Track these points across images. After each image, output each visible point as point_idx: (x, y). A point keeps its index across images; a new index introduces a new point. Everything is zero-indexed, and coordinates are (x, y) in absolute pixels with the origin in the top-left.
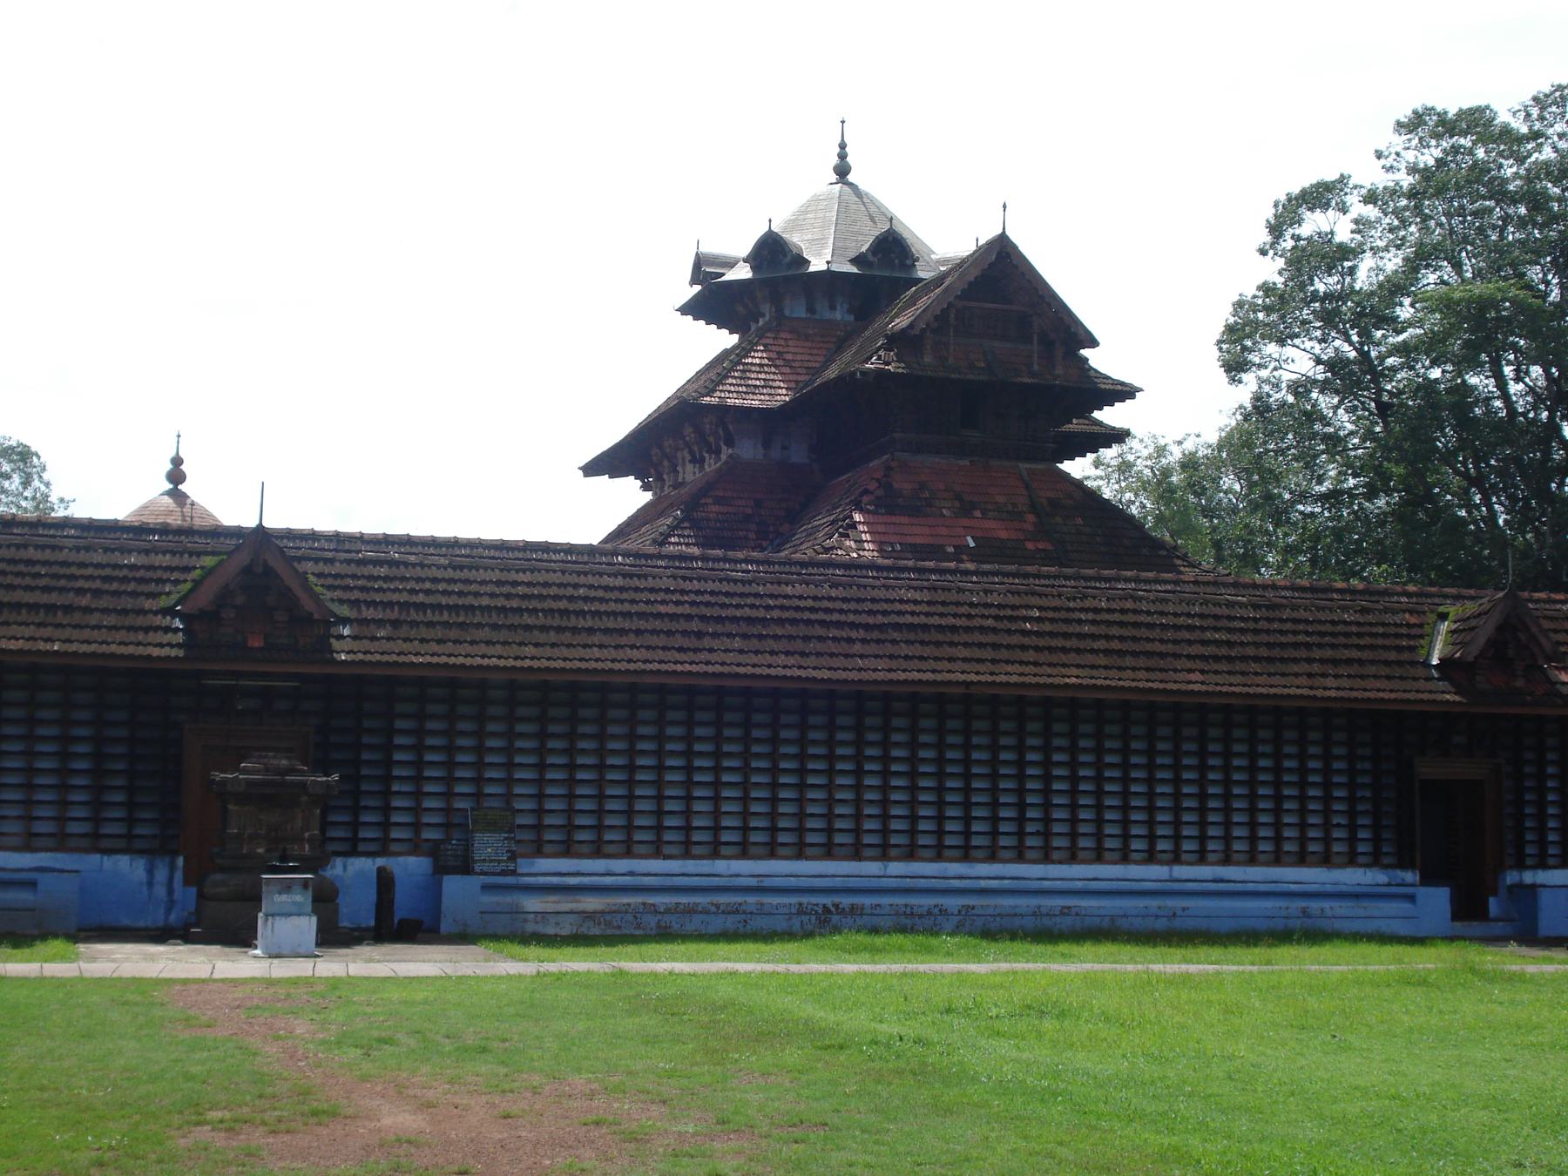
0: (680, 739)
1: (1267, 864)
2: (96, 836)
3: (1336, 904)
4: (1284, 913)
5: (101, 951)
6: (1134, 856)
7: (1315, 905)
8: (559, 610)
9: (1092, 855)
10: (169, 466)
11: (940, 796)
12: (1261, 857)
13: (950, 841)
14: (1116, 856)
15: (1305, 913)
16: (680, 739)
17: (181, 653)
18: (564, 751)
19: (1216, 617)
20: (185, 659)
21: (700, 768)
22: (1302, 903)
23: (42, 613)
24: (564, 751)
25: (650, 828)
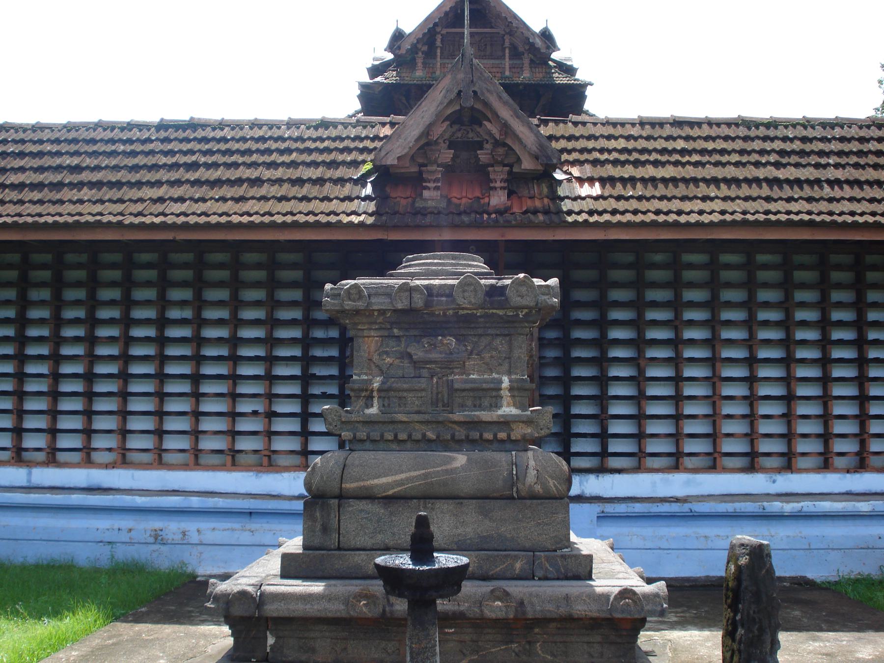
0: (777, 324)
1: (184, 467)
2: (234, 453)
3: (205, 525)
4: (124, 537)
5: (205, 636)
6: (839, 462)
7: (172, 527)
8: (766, 180)
9: (187, 457)
10: (431, 26)
11: (678, 389)
12: (839, 462)
13: (31, 442)
14: (41, 456)
15: (158, 537)
16: (777, 324)
17: (370, 220)
18: (705, 342)
19: (858, 183)
20: (372, 226)
21: (803, 361)
22: (156, 523)
23: (619, 186)
24: (705, 342)
25: (593, 436)
